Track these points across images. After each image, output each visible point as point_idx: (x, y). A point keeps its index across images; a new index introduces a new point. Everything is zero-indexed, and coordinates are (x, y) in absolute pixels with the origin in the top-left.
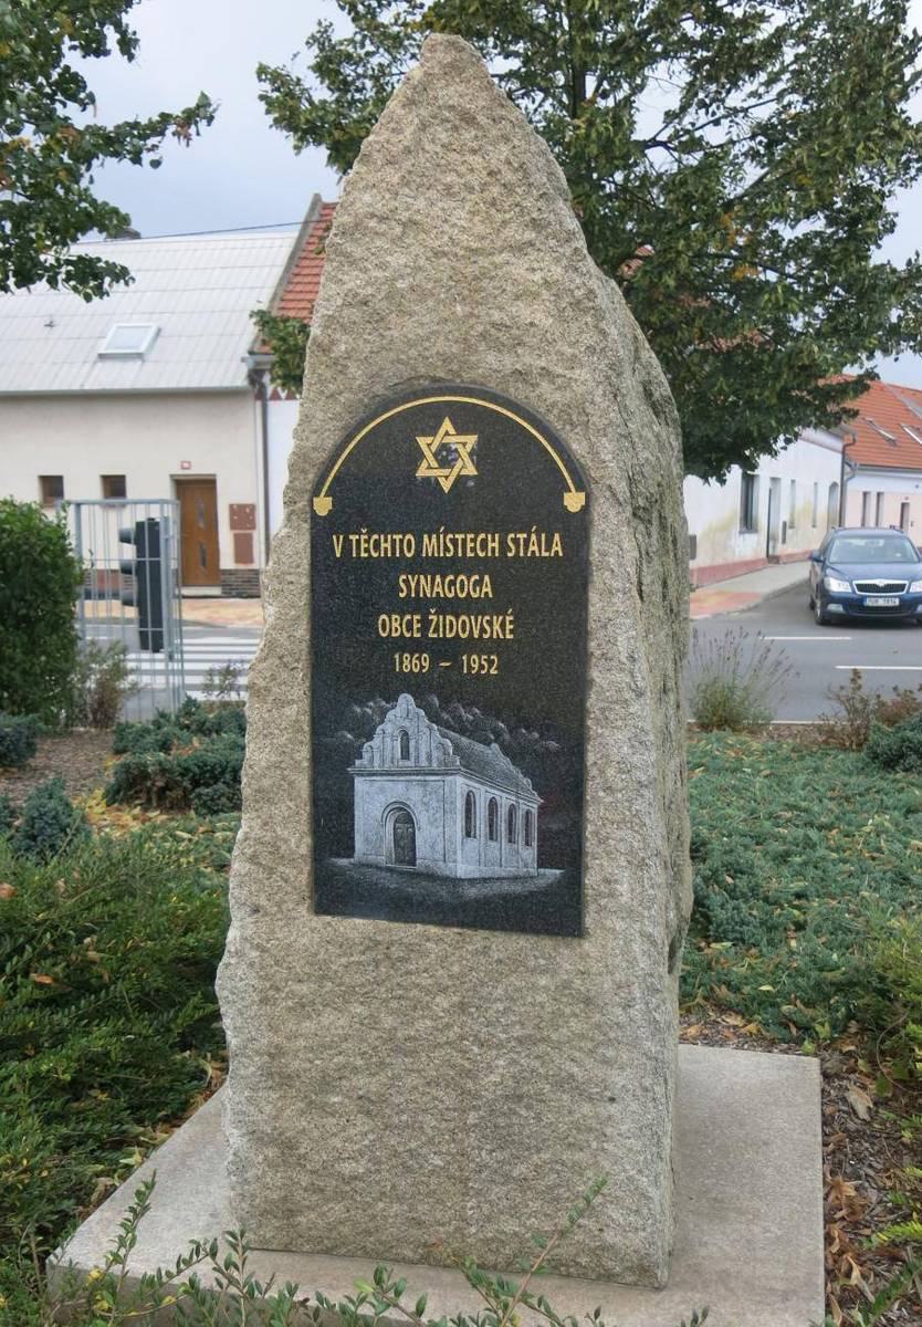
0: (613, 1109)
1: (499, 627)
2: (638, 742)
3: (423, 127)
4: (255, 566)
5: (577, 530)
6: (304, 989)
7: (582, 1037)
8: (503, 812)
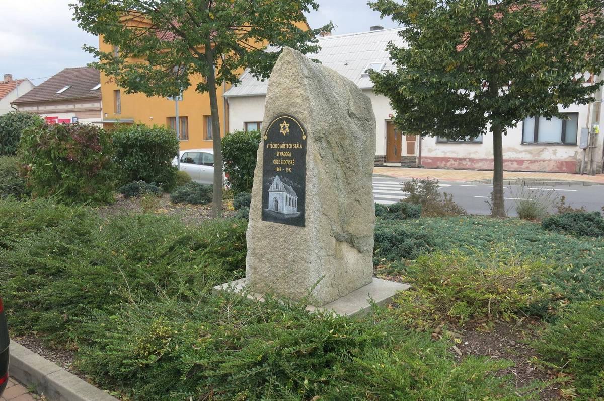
0: (310, 265)
1: (292, 162)
2: (313, 186)
3: (282, 65)
4: (415, 155)
5: (304, 143)
6: (259, 236)
7: (305, 249)
8: (292, 200)
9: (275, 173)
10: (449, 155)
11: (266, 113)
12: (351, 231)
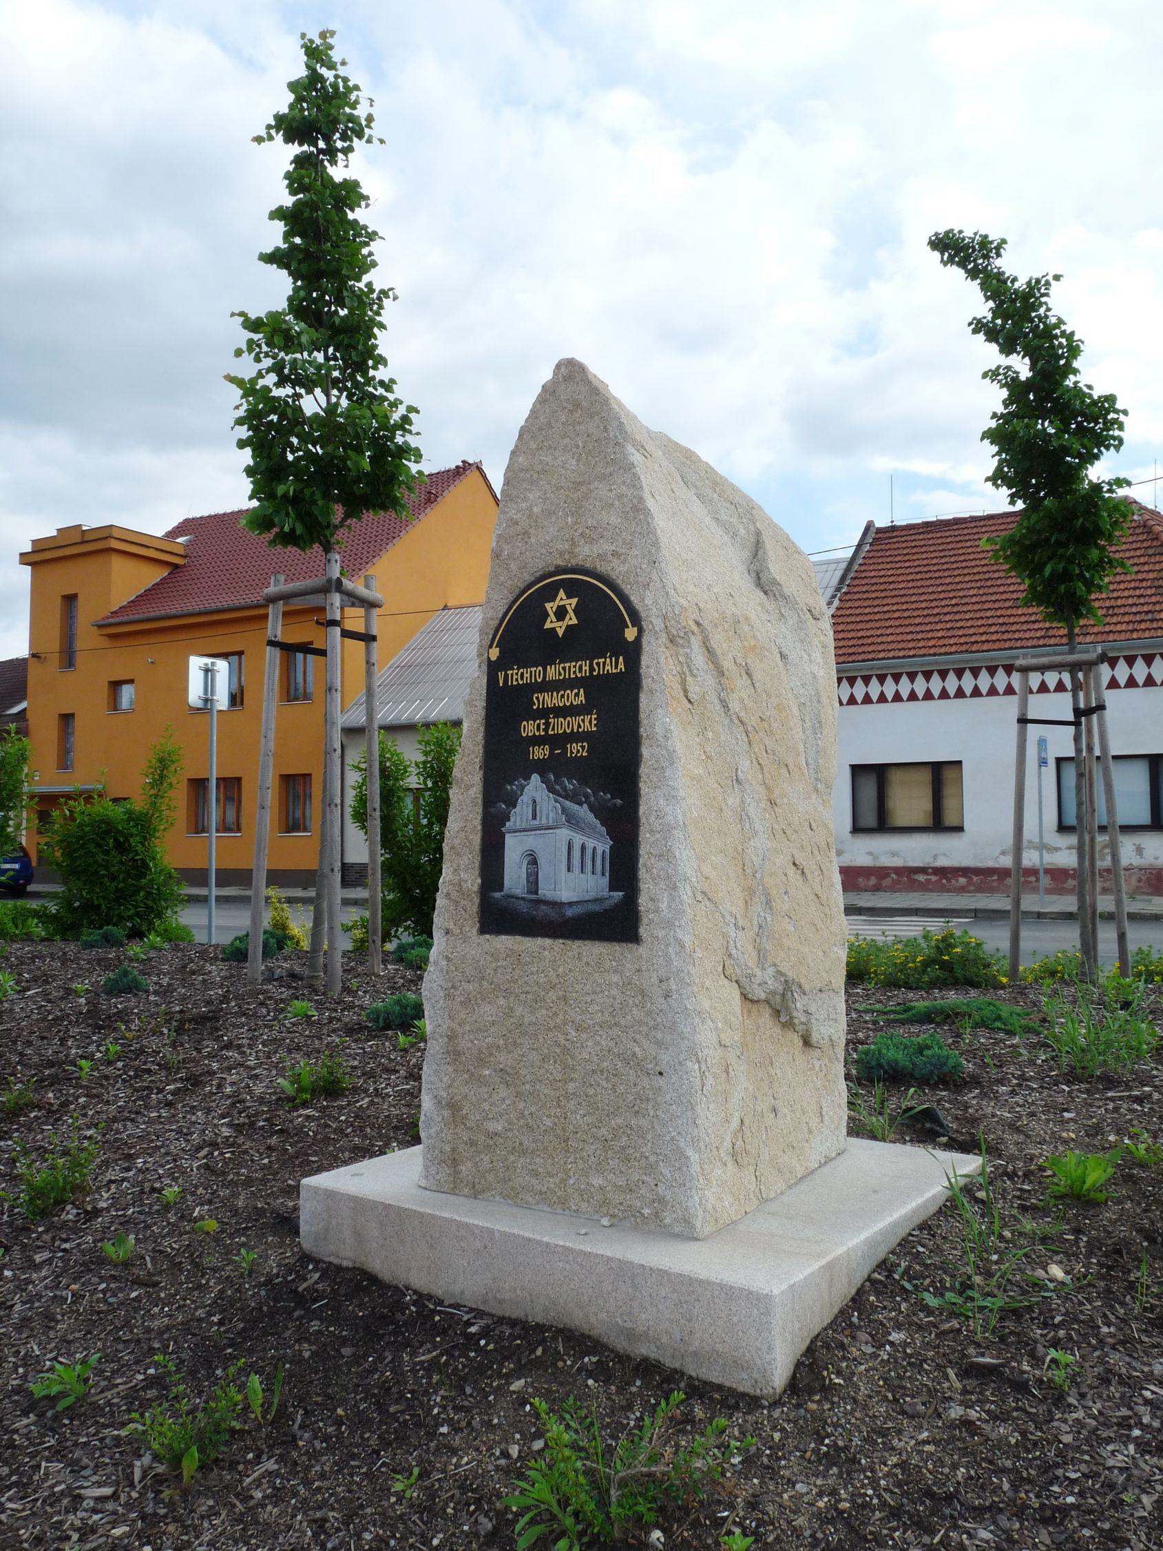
0: (661, 1082)
1: (588, 723)
5: (633, 653)
9: (528, 768)
10: (886, 861)
11: (494, 576)
12: (785, 967)
